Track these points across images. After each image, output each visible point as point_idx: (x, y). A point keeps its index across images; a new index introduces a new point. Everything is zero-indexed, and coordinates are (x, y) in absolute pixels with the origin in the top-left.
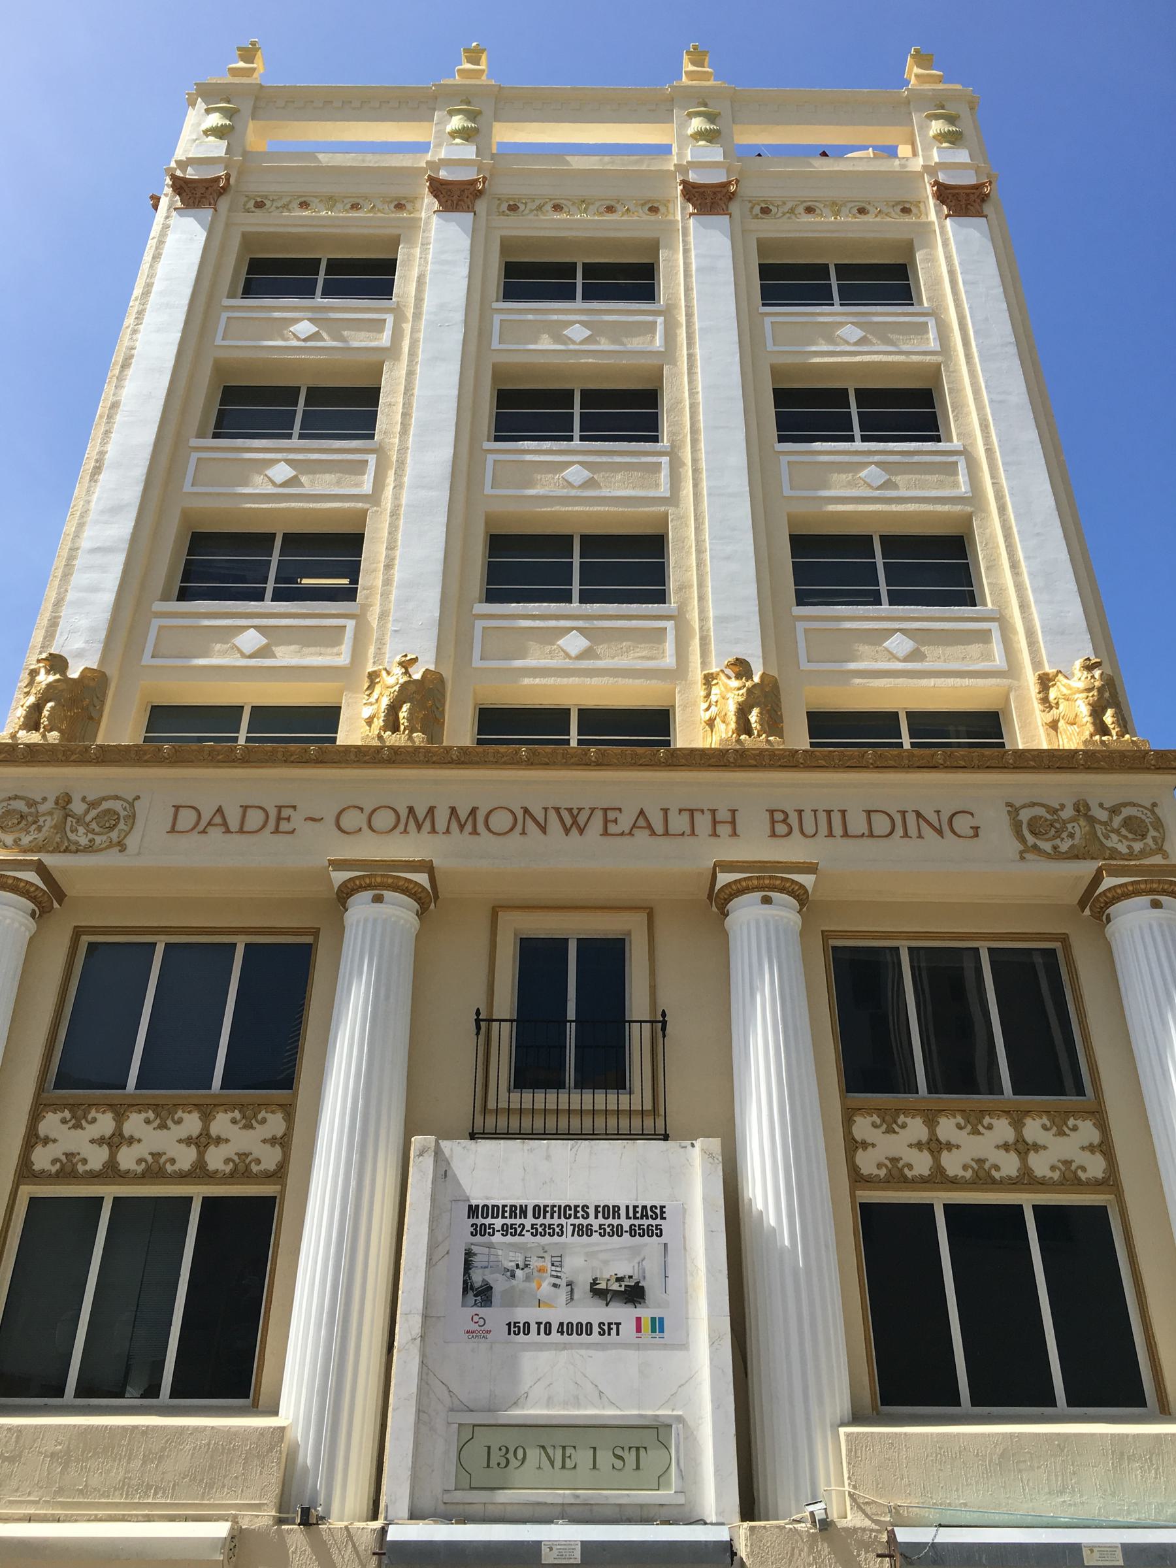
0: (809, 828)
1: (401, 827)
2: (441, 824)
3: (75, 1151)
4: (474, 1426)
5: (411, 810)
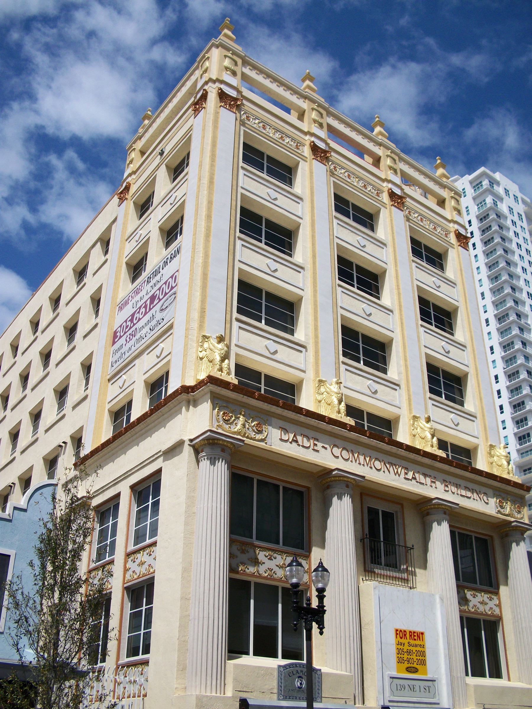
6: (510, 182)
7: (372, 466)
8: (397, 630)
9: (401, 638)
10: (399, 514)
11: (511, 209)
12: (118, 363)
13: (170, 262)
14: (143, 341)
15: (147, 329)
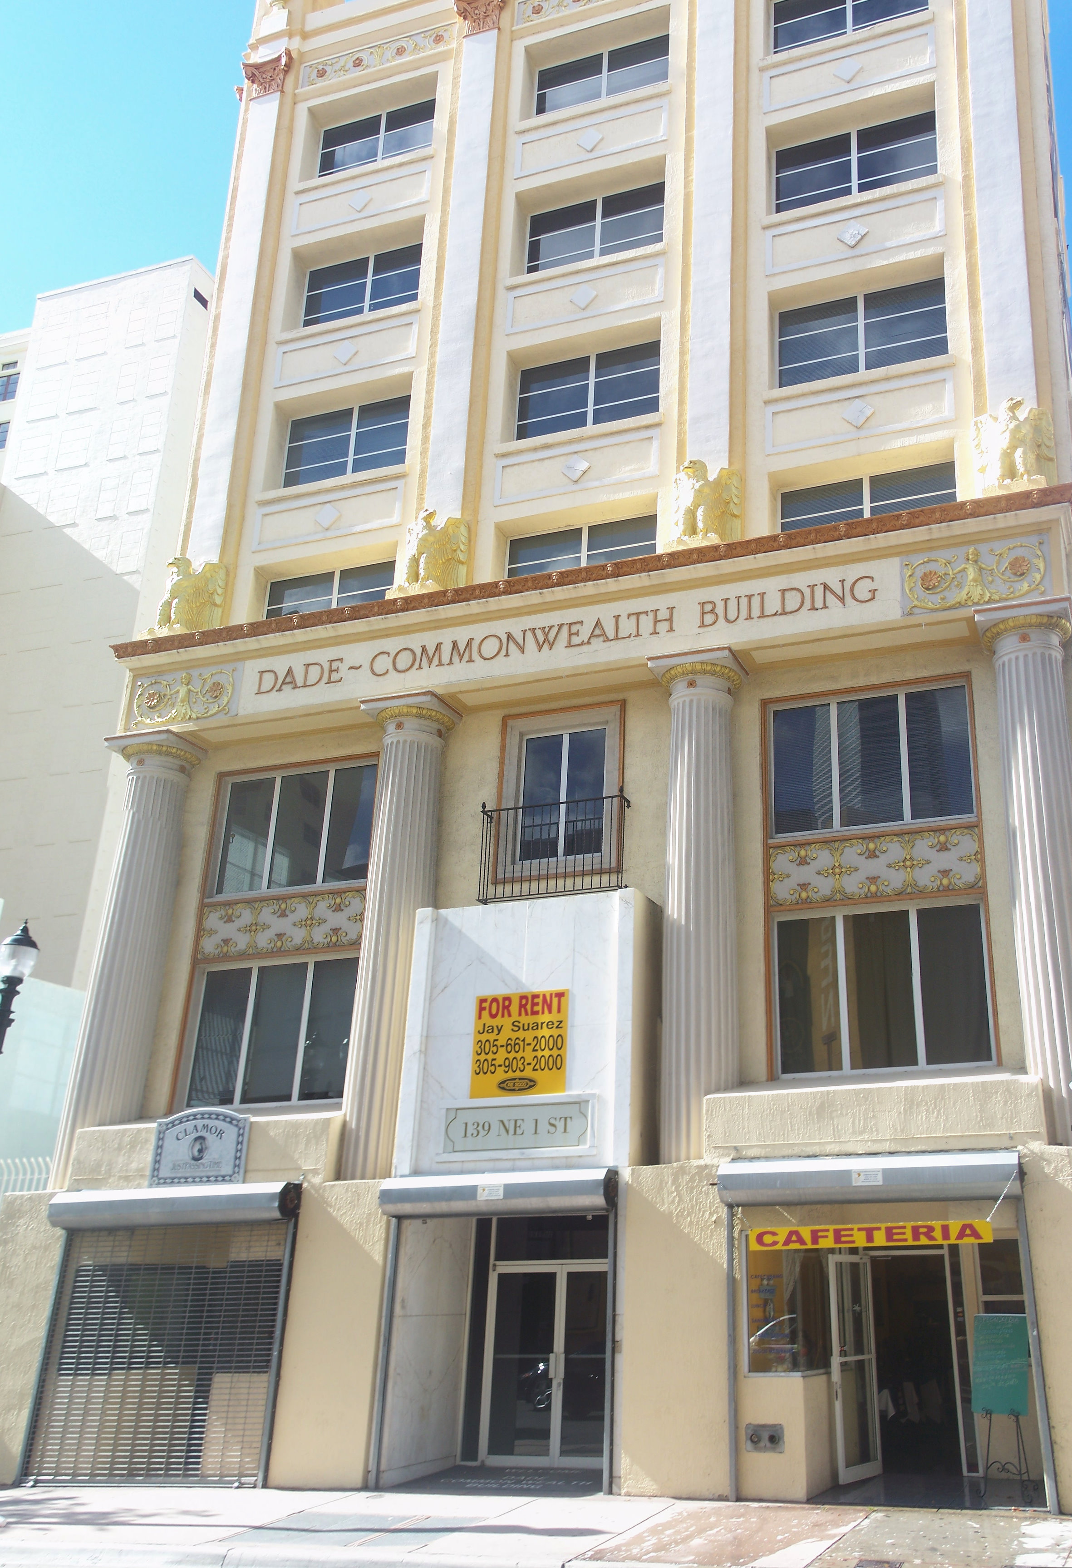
0: (732, 615)
1: (417, 665)
2: (446, 658)
3: (941, 853)
4: (457, 1109)
5: (424, 649)
9: (493, 1016)
10: (611, 744)
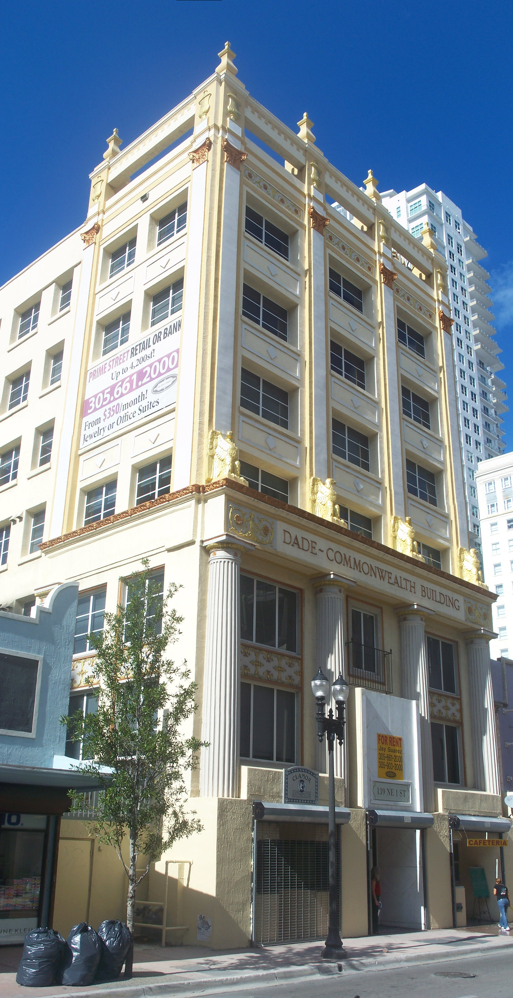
6: (453, 205)
7: (362, 571)
8: (379, 736)
11: (450, 238)
12: (94, 439)
13: (164, 338)
14: (130, 421)
15: (135, 408)
